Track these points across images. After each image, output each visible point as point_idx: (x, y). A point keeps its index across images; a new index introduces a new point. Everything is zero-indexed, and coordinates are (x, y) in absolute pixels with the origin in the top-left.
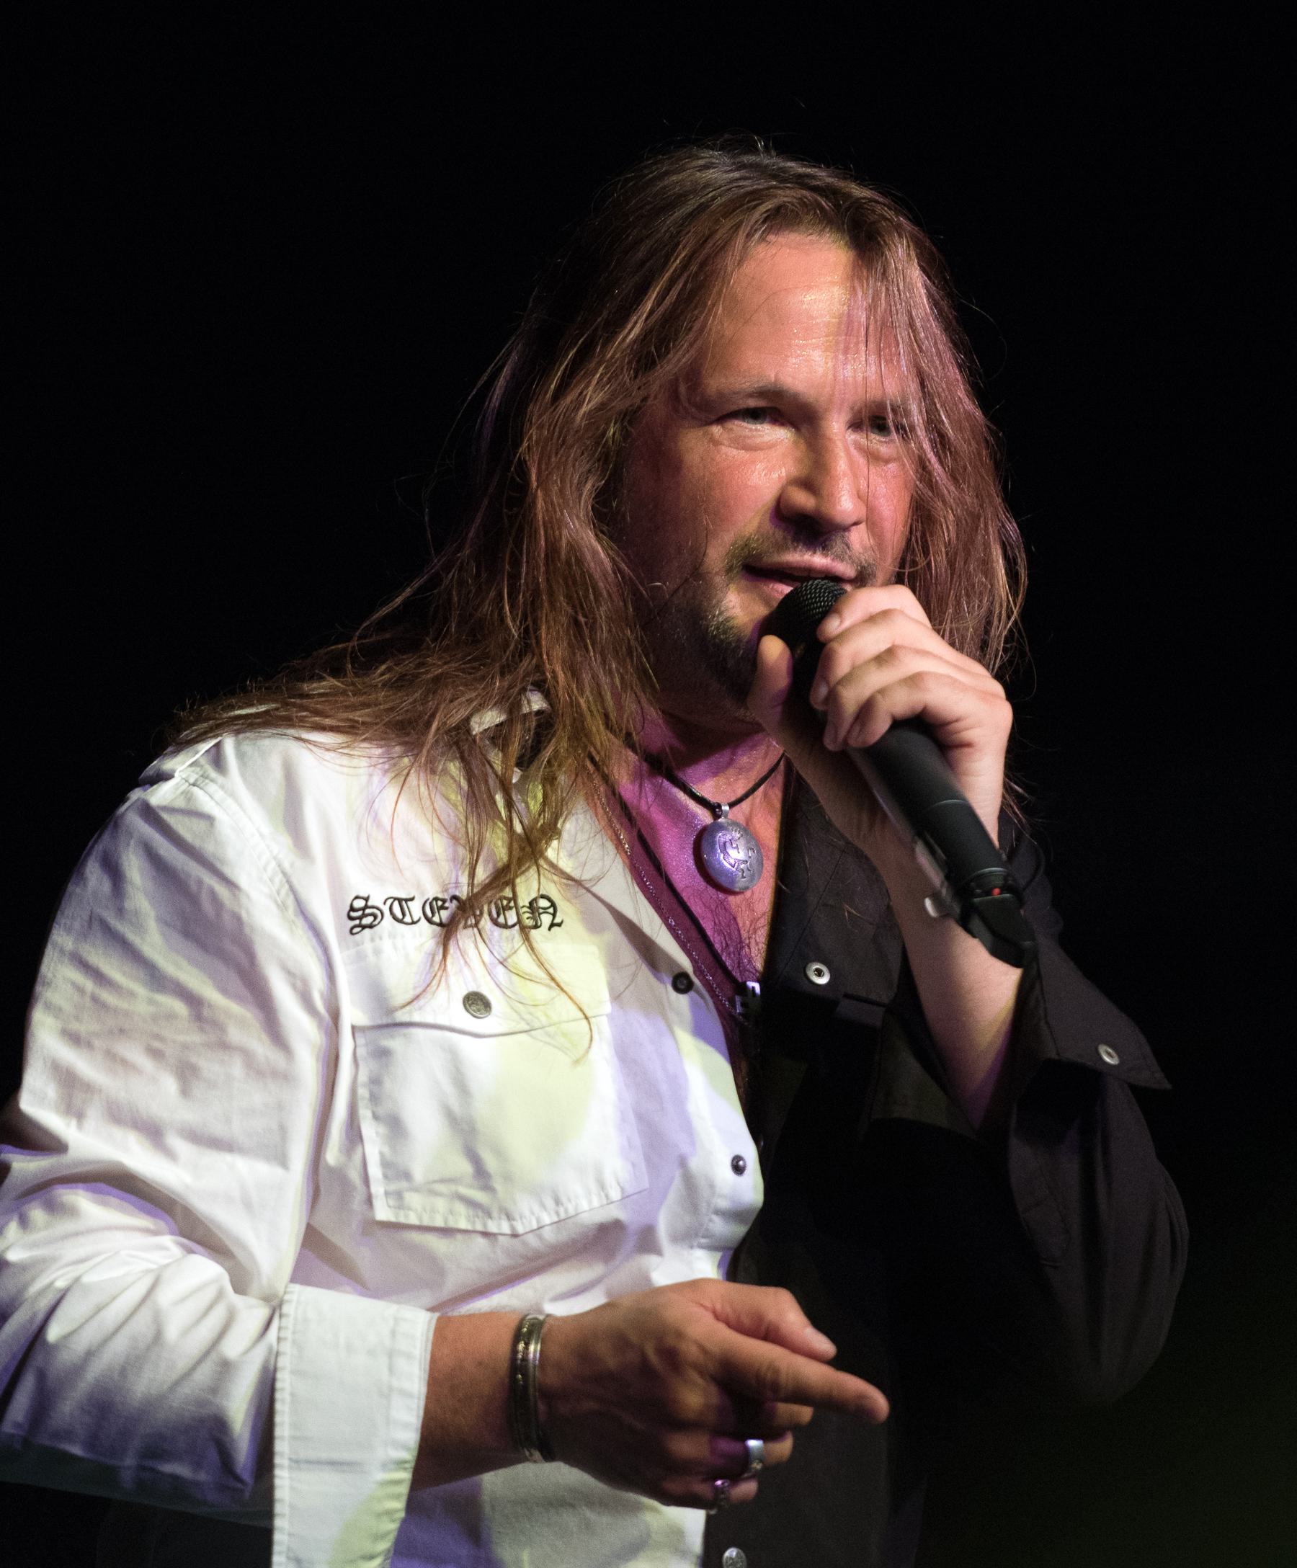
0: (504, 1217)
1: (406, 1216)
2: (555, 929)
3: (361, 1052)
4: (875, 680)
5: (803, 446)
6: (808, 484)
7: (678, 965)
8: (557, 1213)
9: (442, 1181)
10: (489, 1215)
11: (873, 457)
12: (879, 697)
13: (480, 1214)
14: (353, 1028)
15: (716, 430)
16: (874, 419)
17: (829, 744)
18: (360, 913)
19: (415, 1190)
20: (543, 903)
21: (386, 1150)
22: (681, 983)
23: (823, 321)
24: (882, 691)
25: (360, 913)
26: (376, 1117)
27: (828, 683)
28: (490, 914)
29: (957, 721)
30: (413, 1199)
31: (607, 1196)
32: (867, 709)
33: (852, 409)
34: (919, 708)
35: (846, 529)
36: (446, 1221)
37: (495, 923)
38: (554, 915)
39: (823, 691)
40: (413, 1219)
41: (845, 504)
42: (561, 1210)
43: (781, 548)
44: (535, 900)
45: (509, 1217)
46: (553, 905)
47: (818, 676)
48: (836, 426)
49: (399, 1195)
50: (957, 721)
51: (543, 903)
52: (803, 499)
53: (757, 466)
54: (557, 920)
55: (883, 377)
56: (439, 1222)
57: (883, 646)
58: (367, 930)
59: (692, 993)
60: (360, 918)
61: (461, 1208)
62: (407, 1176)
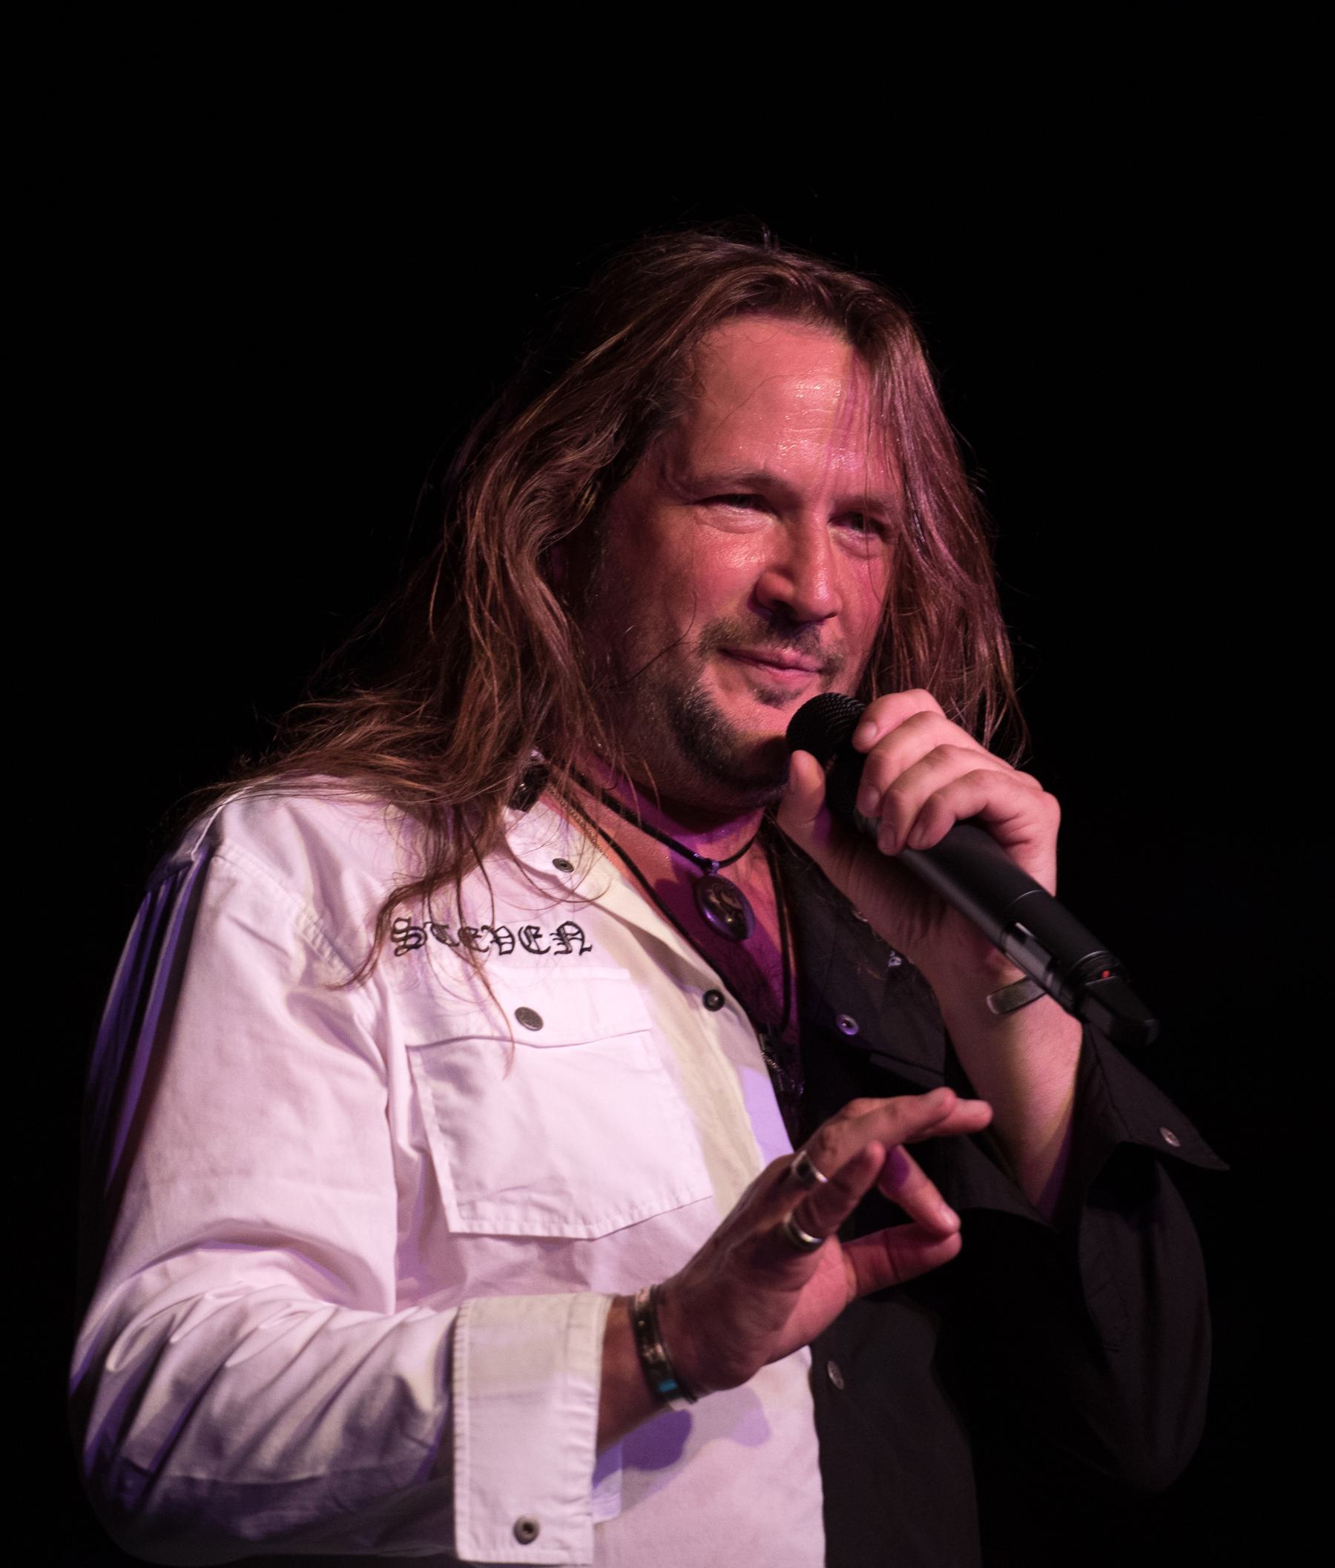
0: (580, 1221)
1: (480, 1226)
2: (585, 953)
3: (419, 1070)
4: (930, 782)
5: (784, 534)
6: (787, 572)
7: (711, 983)
8: (632, 1216)
9: (514, 1189)
10: (566, 1220)
11: (851, 551)
12: (940, 797)
13: (556, 1219)
14: (408, 1048)
15: (701, 512)
16: (851, 514)
17: (886, 846)
18: (403, 935)
19: (489, 1199)
20: (569, 929)
21: (455, 1161)
22: (712, 1001)
23: (806, 402)
24: (942, 791)
25: (403, 935)
26: (444, 1130)
27: (878, 789)
28: (522, 943)
29: (1015, 817)
30: (488, 1209)
31: (677, 1199)
32: (927, 811)
33: (836, 502)
34: (981, 807)
35: (821, 620)
36: (521, 1228)
37: (527, 948)
38: (583, 940)
39: (874, 797)
40: (488, 1229)
41: (821, 593)
42: (635, 1212)
43: (757, 638)
44: (562, 926)
45: (585, 1222)
46: (580, 931)
47: (864, 781)
48: (818, 517)
49: (472, 1205)
50: (1015, 817)
51: (569, 929)
52: (783, 587)
53: (738, 550)
54: (587, 945)
55: (858, 469)
56: (514, 1231)
57: (930, 748)
58: (413, 951)
59: (724, 1009)
60: (405, 939)
61: (535, 1214)
62: (480, 1185)
